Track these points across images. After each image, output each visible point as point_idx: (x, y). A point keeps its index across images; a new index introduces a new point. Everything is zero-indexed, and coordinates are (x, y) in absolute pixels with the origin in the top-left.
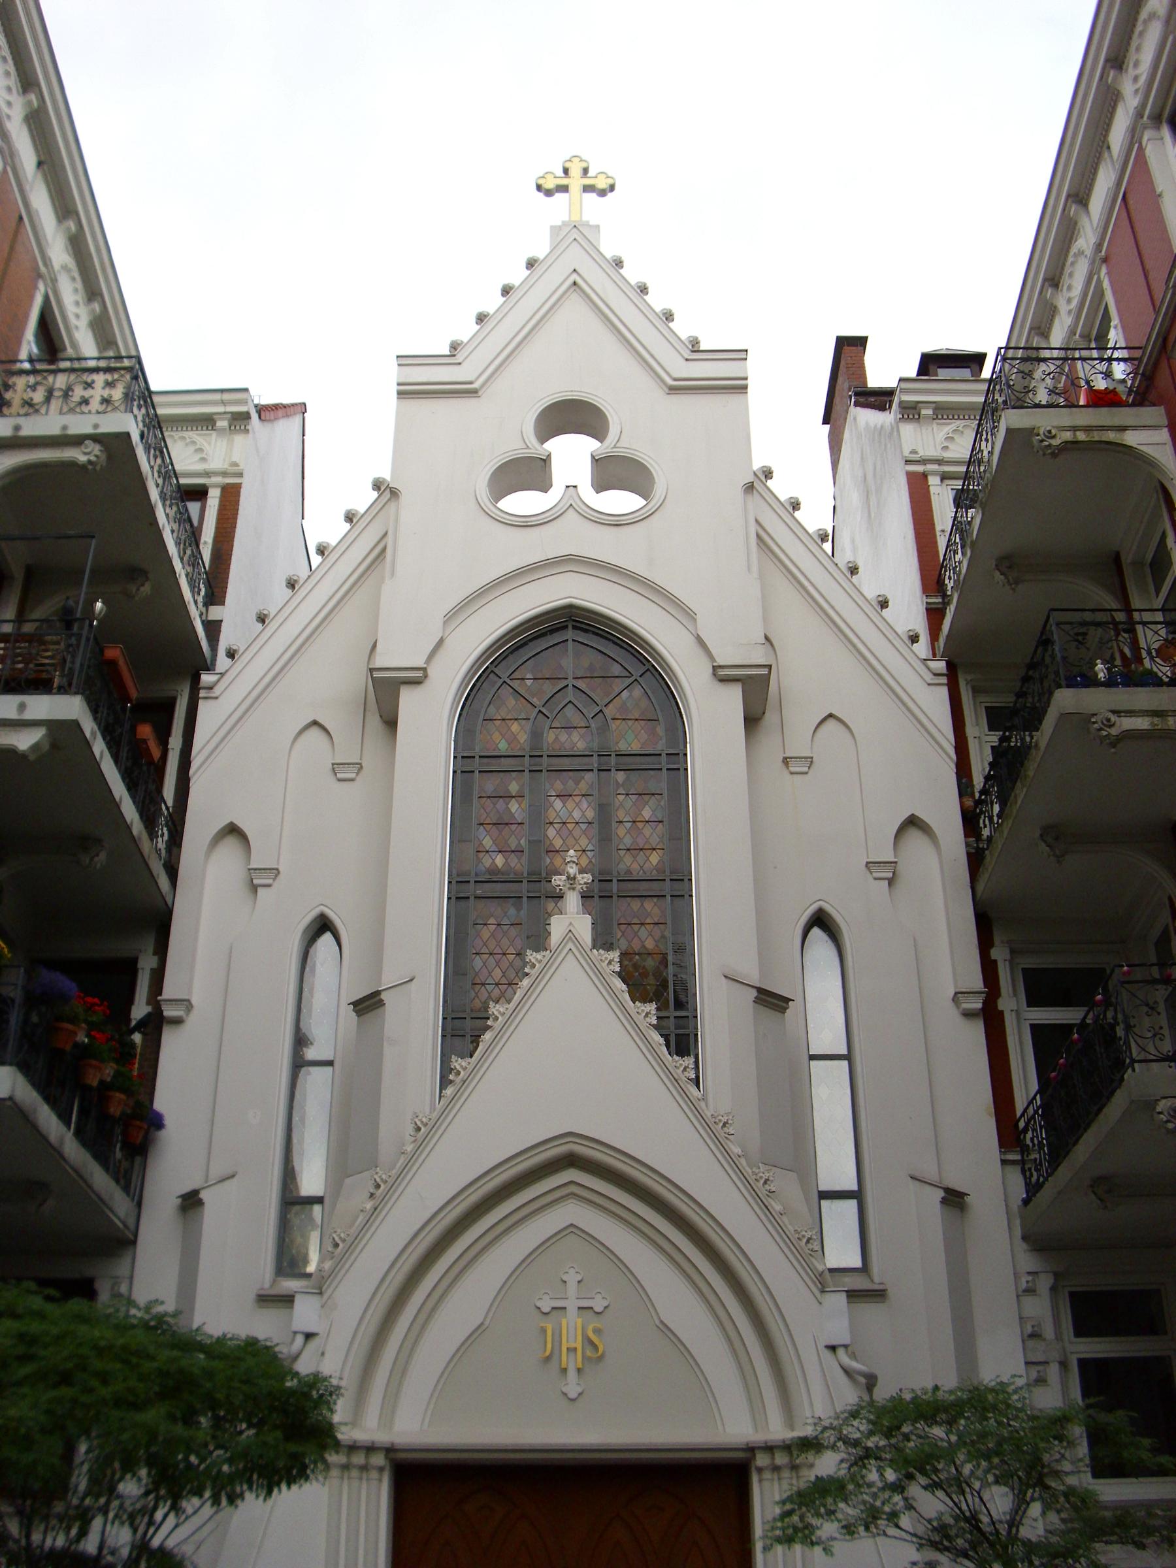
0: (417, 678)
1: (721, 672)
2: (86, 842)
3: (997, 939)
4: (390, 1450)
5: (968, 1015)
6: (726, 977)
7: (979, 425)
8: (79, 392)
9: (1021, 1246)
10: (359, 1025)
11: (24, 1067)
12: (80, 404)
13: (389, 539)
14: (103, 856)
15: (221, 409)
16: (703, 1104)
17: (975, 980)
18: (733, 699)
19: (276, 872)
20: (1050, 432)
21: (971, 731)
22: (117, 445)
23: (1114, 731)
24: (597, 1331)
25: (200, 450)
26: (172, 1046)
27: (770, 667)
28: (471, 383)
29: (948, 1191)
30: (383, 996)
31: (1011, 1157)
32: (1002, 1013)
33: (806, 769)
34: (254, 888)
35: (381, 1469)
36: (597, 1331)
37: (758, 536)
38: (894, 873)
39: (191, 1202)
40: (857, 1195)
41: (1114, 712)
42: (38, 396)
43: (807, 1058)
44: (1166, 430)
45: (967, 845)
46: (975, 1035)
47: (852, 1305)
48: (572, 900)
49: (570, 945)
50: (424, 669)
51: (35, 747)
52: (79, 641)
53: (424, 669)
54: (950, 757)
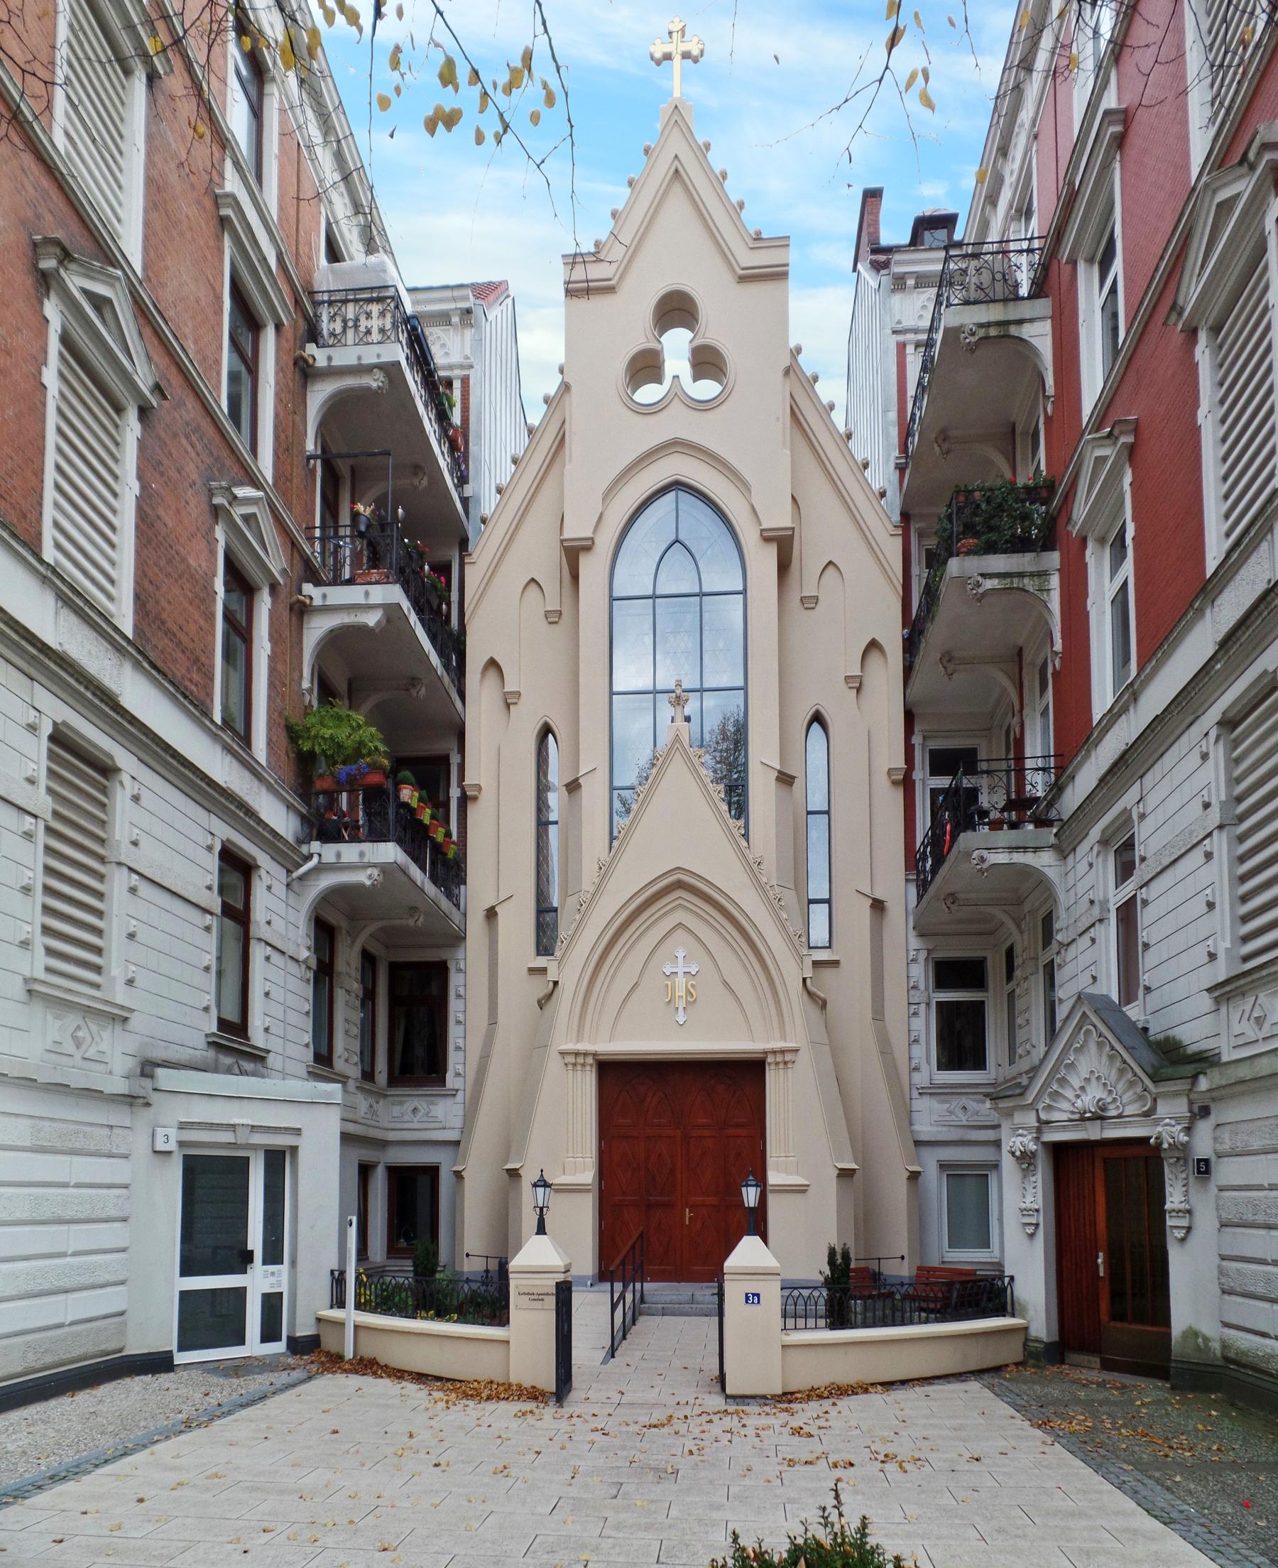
0: (587, 546)
1: (765, 534)
2: (414, 681)
3: (916, 729)
4: (595, 1055)
5: (894, 783)
7: (939, 295)
9: (912, 933)
10: (570, 800)
11: (400, 842)
13: (567, 426)
14: (423, 689)
15: (452, 306)
16: (747, 850)
17: (900, 763)
18: (772, 552)
19: (519, 694)
20: (971, 330)
21: (915, 570)
22: (391, 370)
23: (981, 590)
24: (693, 986)
26: (475, 814)
27: (793, 529)
28: (609, 280)
29: (874, 899)
30: (581, 781)
31: (911, 877)
33: (813, 605)
34: (508, 706)
35: (591, 1065)
36: (693, 986)
38: (861, 684)
39: (491, 914)
40: (828, 901)
41: (982, 575)
43: (805, 813)
44: (1049, 321)
45: (904, 659)
46: (899, 795)
47: (1039, 830)
49: (677, 745)
50: (592, 539)
51: (378, 622)
52: (392, 540)
53: (592, 539)
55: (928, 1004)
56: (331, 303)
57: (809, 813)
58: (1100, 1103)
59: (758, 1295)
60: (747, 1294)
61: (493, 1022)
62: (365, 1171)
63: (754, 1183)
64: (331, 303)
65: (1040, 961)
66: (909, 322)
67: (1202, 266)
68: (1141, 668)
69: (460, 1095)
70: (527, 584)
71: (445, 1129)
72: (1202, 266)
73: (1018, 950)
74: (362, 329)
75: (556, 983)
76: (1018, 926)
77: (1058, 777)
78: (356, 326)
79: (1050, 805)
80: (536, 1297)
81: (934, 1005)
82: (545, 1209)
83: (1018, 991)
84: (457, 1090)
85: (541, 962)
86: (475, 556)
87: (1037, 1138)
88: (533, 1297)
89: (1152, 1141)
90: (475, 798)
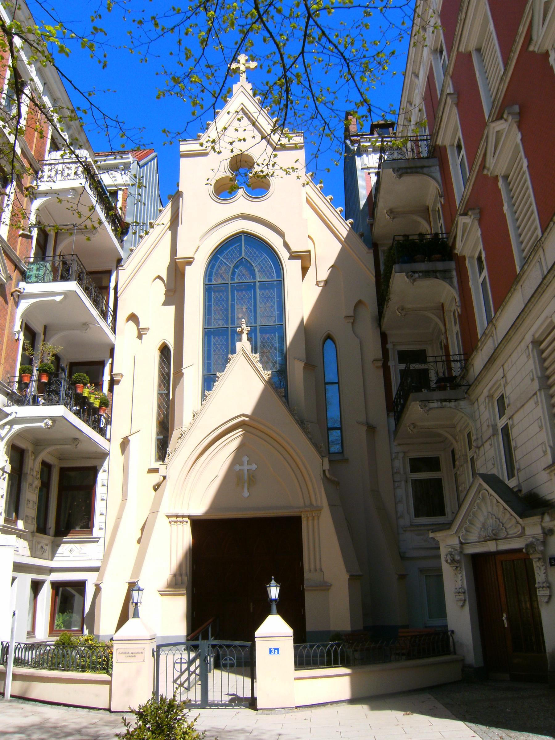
4: (189, 517)
5: (377, 367)
6: (306, 193)
8: (66, 172)
12: (68, 175)
25: (114, 177)
32: (389, 367)
37: (307, 199)
40: (340, 429)
42: (53, 173)
48: (244, 337)
54: (372, 274)
55: (406, 482)
56: (50, 164)
57: (326, 384)
58: (494, 532)
59: (278, 649)
60: (270, 649)
61: (124, 498)
62: (36, 586)
63: (275, 585)
64: (50, 164)
65: (468, 456)
66: (371, 165)
67: (494, 153)
68: (495, 313)
69: (101, 541)
70: (155, 279)
71: (91, 560)
72: (494, 153)
73: (456, 451)
74: (66, 174)
75: (165, 477)
76: (455, 439)
77: (465, 364)
78: (62, 173)
79: (463, 378)
80: (130, 655)
81: (410, 481)
82: (139, 604)
83: (458, 473)
84: (99, 538)
85: (157, 465)
86: (125, 267)
87: (461, 552)
88: (129, 655)
89: (524, 550)
90: (118, 382)
